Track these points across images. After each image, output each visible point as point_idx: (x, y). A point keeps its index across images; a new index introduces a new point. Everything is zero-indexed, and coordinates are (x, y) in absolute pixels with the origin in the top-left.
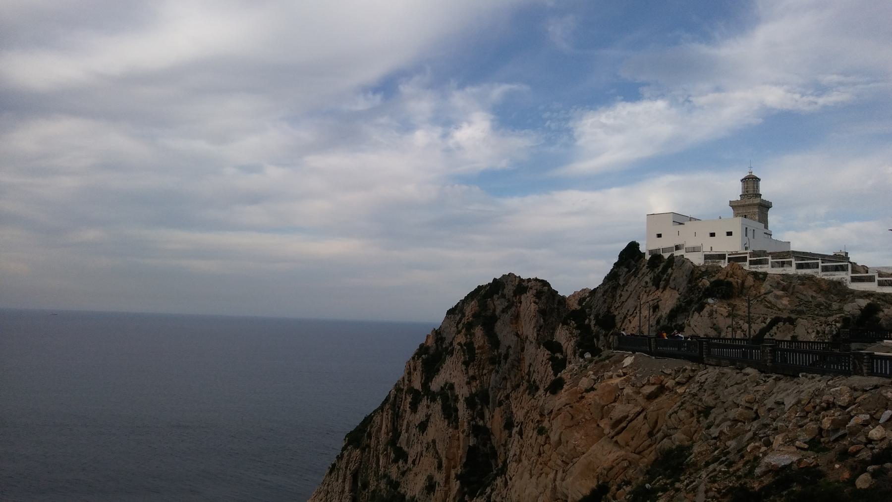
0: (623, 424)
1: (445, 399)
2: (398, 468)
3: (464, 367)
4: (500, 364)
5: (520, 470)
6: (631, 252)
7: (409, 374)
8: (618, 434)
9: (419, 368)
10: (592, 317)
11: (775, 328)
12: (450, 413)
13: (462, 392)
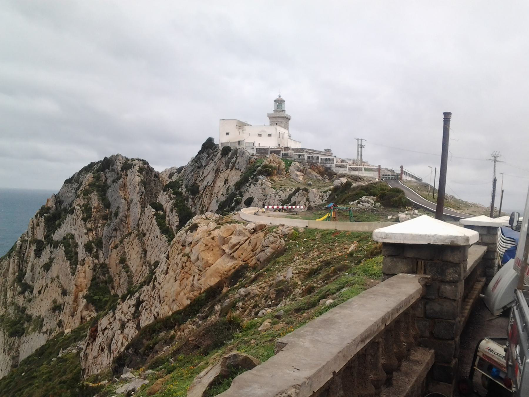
0: (237, 247)
1: (67, 246)
2: (25, 298)
3: (83, 222)
4: (111, 219)
5: (167, 279)
6: (209, 145)
7: (33, 228)
8: (234, 252)
9: (42, 224)
10: (183, 186)
11: (297, 194)
12: (71, 256)
13: (82, 240)
